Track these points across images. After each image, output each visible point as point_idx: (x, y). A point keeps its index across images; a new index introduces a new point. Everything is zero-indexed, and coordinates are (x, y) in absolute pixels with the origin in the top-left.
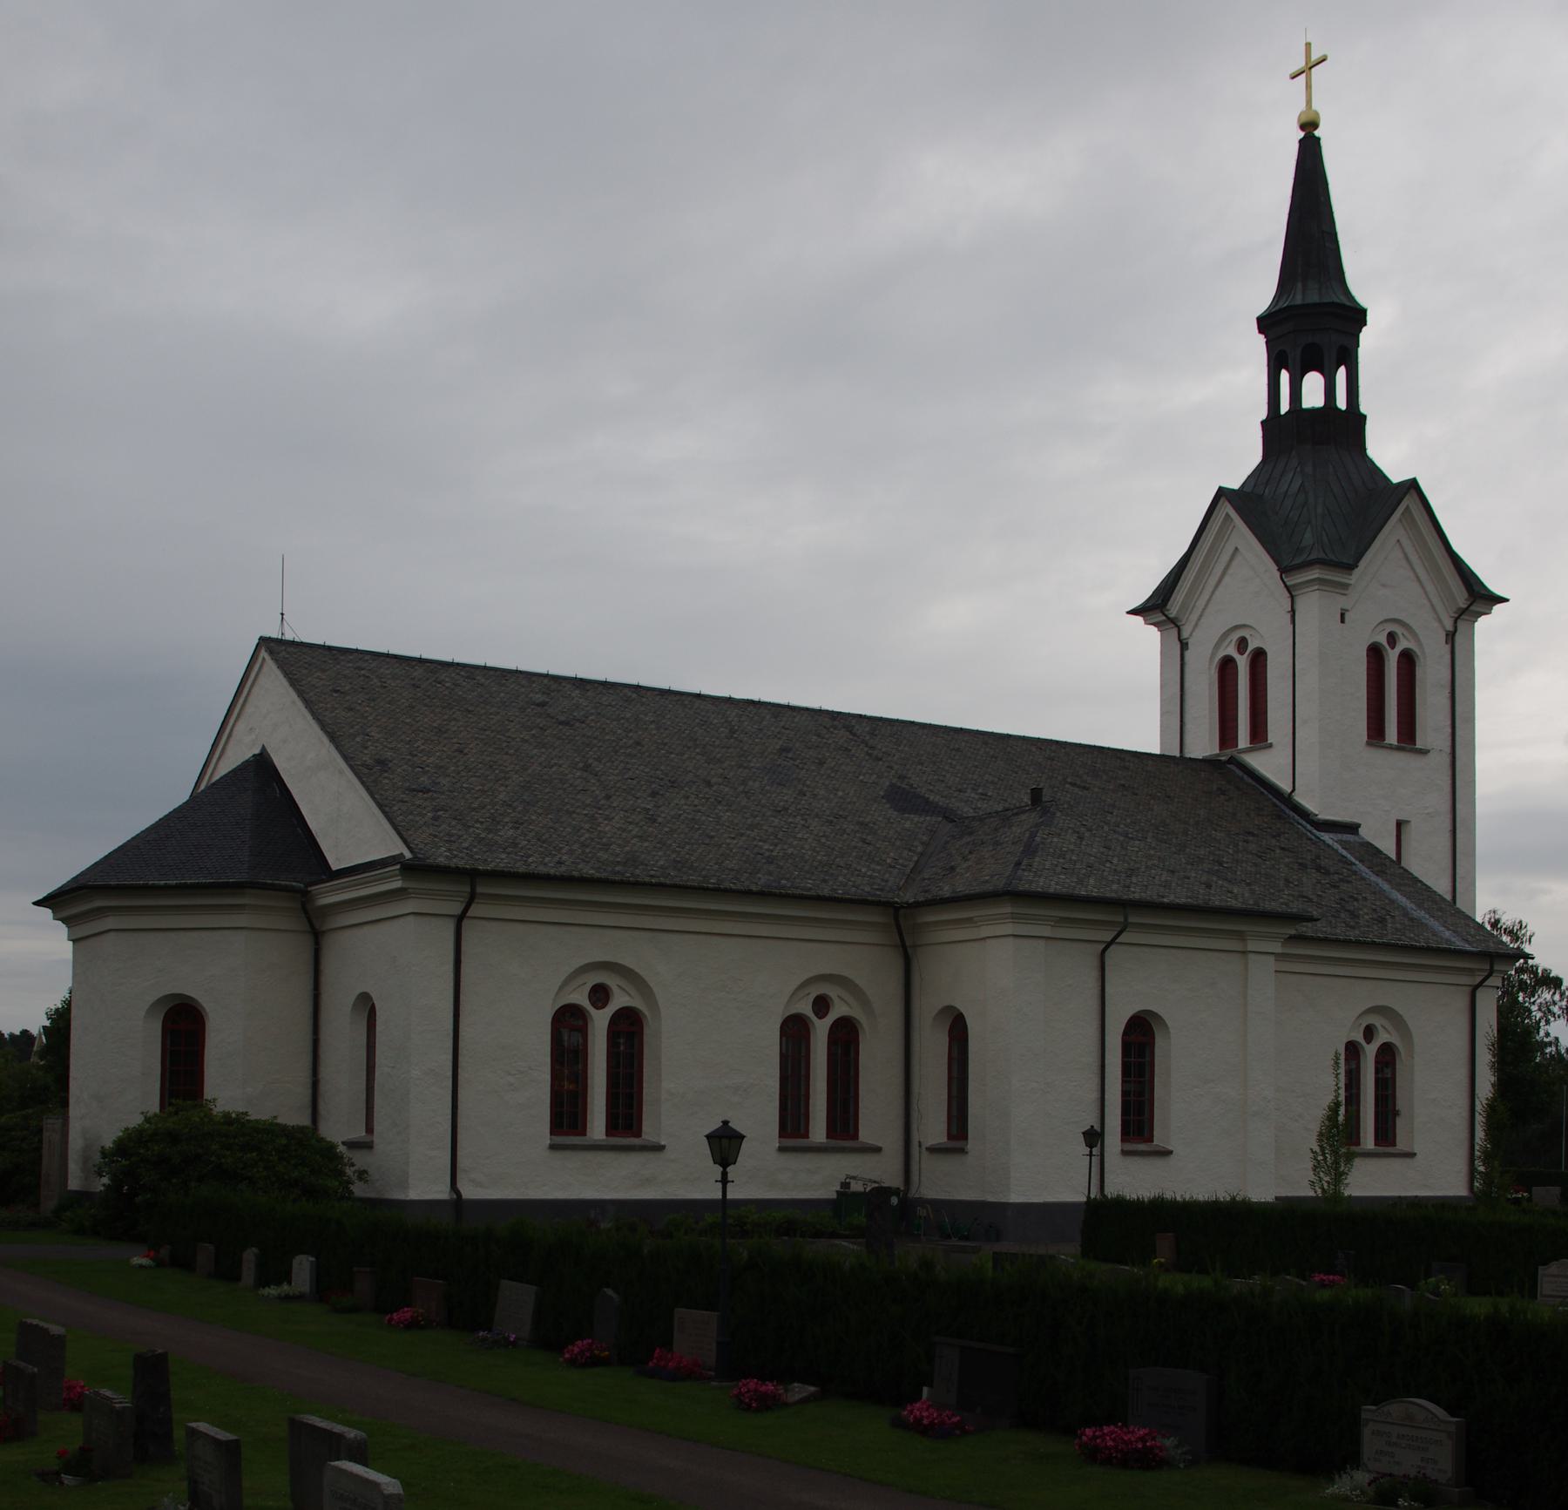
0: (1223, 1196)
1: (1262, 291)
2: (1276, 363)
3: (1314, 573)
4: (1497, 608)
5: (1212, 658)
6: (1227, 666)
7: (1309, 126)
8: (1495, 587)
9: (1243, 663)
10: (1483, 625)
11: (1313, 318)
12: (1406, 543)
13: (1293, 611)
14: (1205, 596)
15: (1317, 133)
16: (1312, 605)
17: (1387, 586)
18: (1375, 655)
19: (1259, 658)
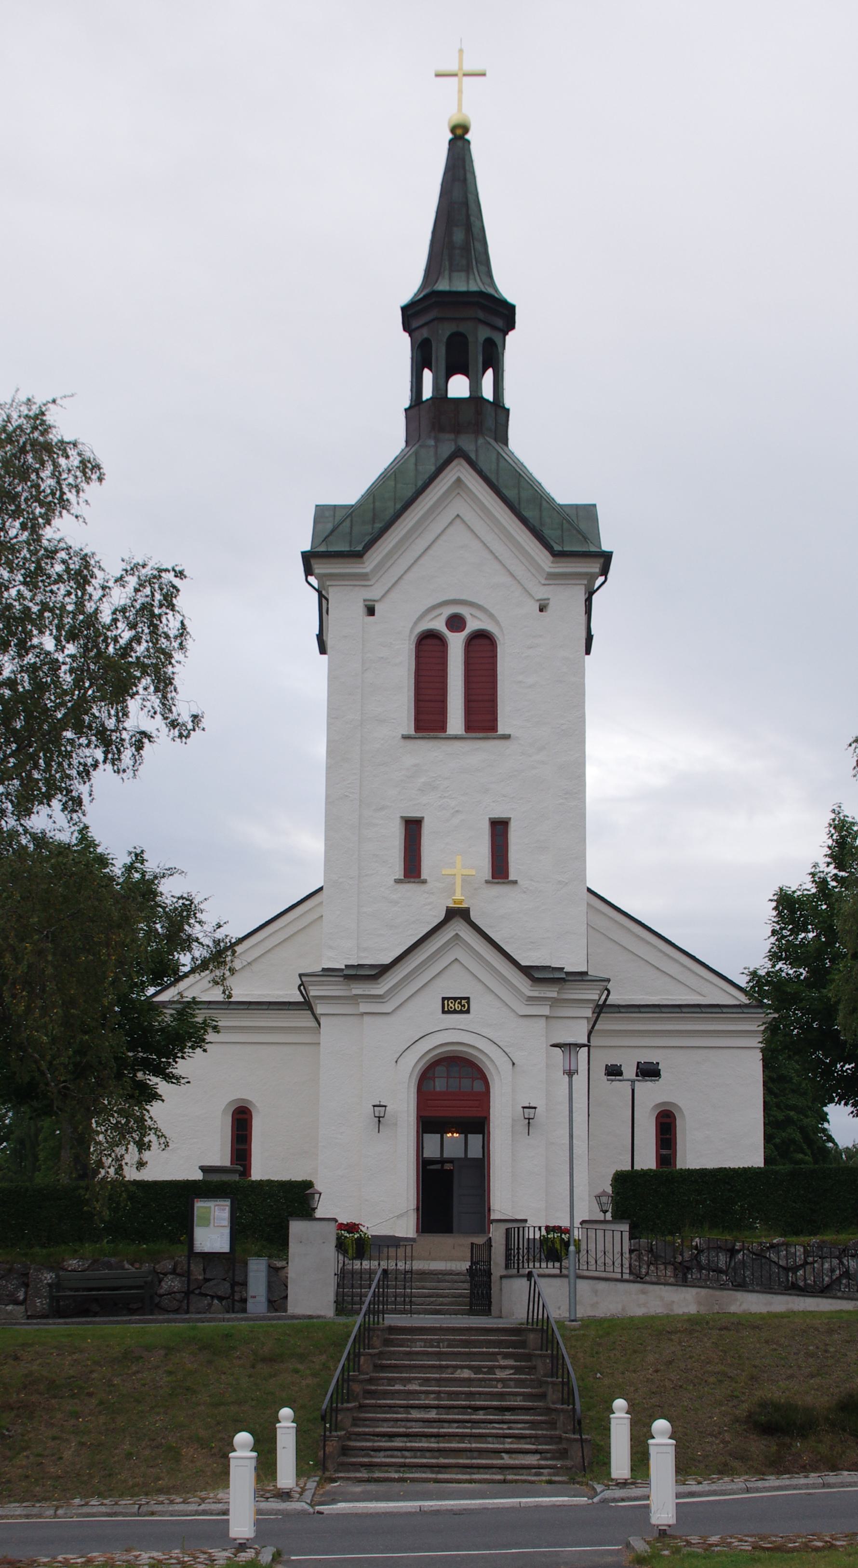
1: (408, 279)
11: (458, 319)
12: (469, 516)
15: (467, 137)
18: (430, 646)
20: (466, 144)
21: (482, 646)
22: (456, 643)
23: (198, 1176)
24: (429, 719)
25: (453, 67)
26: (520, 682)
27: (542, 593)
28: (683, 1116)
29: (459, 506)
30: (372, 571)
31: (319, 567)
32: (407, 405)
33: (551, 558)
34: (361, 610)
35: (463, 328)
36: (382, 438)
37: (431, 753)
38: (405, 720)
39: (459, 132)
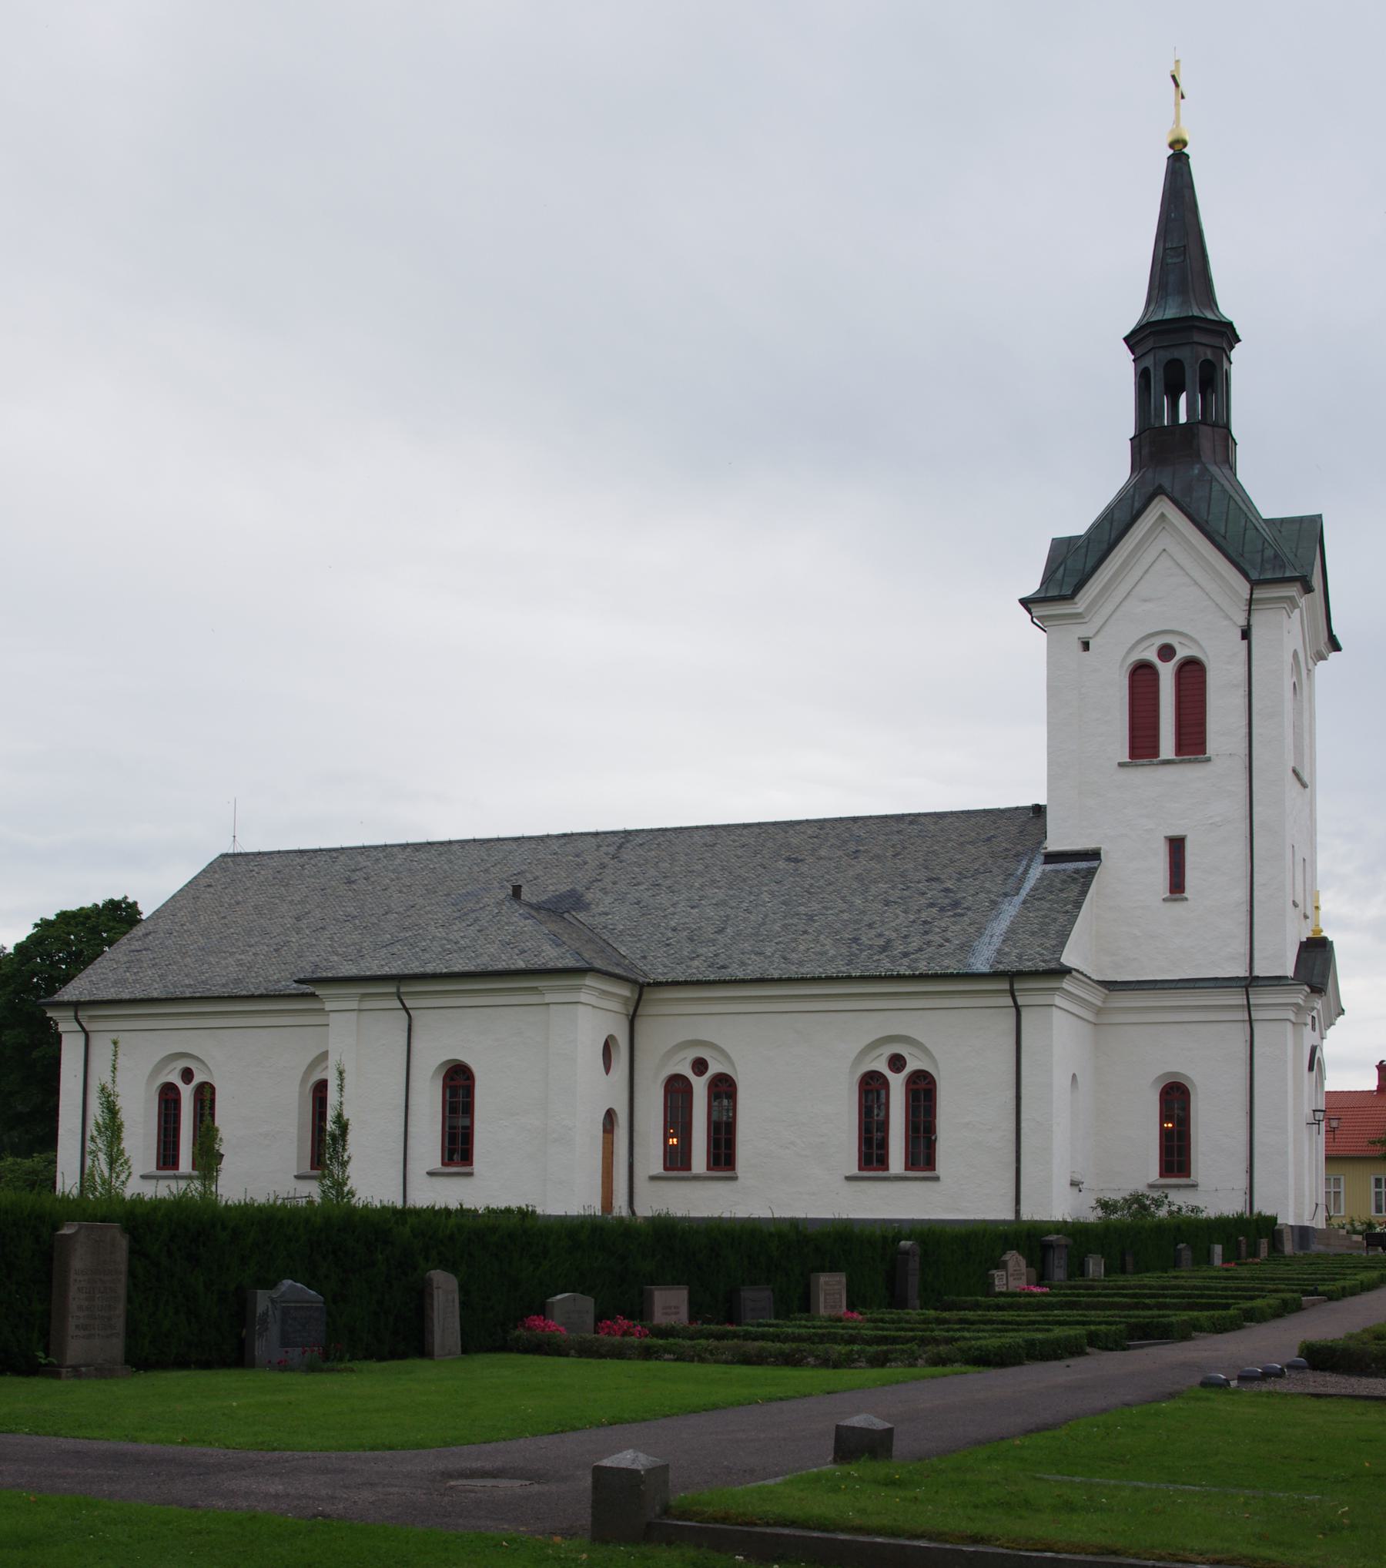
1: (1131, 309)
2: (1143, 380)
5: (1121, 666)
7: (1178, 164)
9: (187, 1093)
11: (1182, 348)
15: (1186, 150)
18: (1142, 676)
23: (1092, 1216)
24: (1142, 745)
28: (1187, 1078)
29: (1165, 541)
30: (1089, 608)
31: (1038, 611)
32: (1132, 435)
34: (1078, 646)
35: (1177, 354)
36: (1110, 471)
37: (1146, 777)
38: (1121, 749)
39: (1177, 147)
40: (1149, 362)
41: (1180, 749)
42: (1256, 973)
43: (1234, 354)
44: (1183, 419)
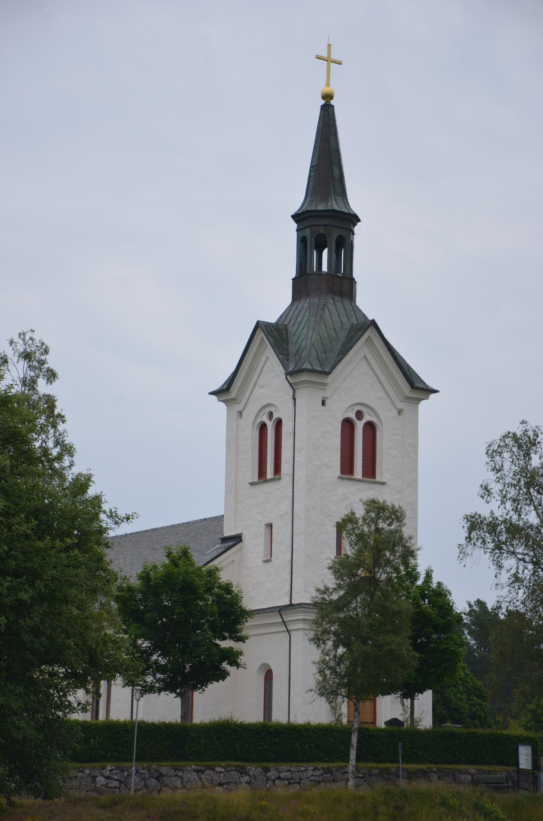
0: (217, 719)
1: (296, 199)
2: (302, 242)
3: (305, 377)
4: (432, 396)
5: (253, 426)
6: (263, 427)
7: (328, 97)
8: (431, 383)
10: (423, 405)
11: (325, 226)
12: (370, 357)
13: (294, 399)
14: (248, 392)
15: (332, 102)
16: (308, 398)
17: (356, 384)
18: (348, 425)
19: (279, 423)
20: (331, 108)
21: (370, 428)
22: (359, 426)
25: (325, 55)
26: (389, 454)
27: (400, 405)
33: (410, 389)
40: (307, 233)
41: (364, 475)
42: (294, 602)
43: (356, 229)
44: (325, 268)
